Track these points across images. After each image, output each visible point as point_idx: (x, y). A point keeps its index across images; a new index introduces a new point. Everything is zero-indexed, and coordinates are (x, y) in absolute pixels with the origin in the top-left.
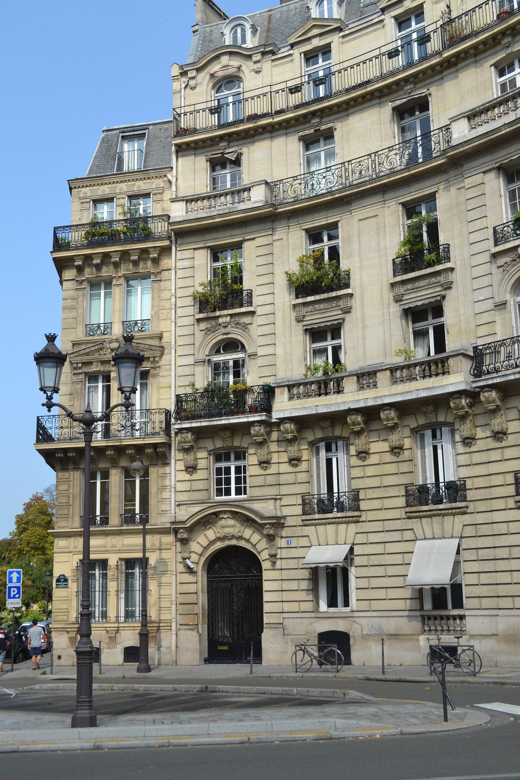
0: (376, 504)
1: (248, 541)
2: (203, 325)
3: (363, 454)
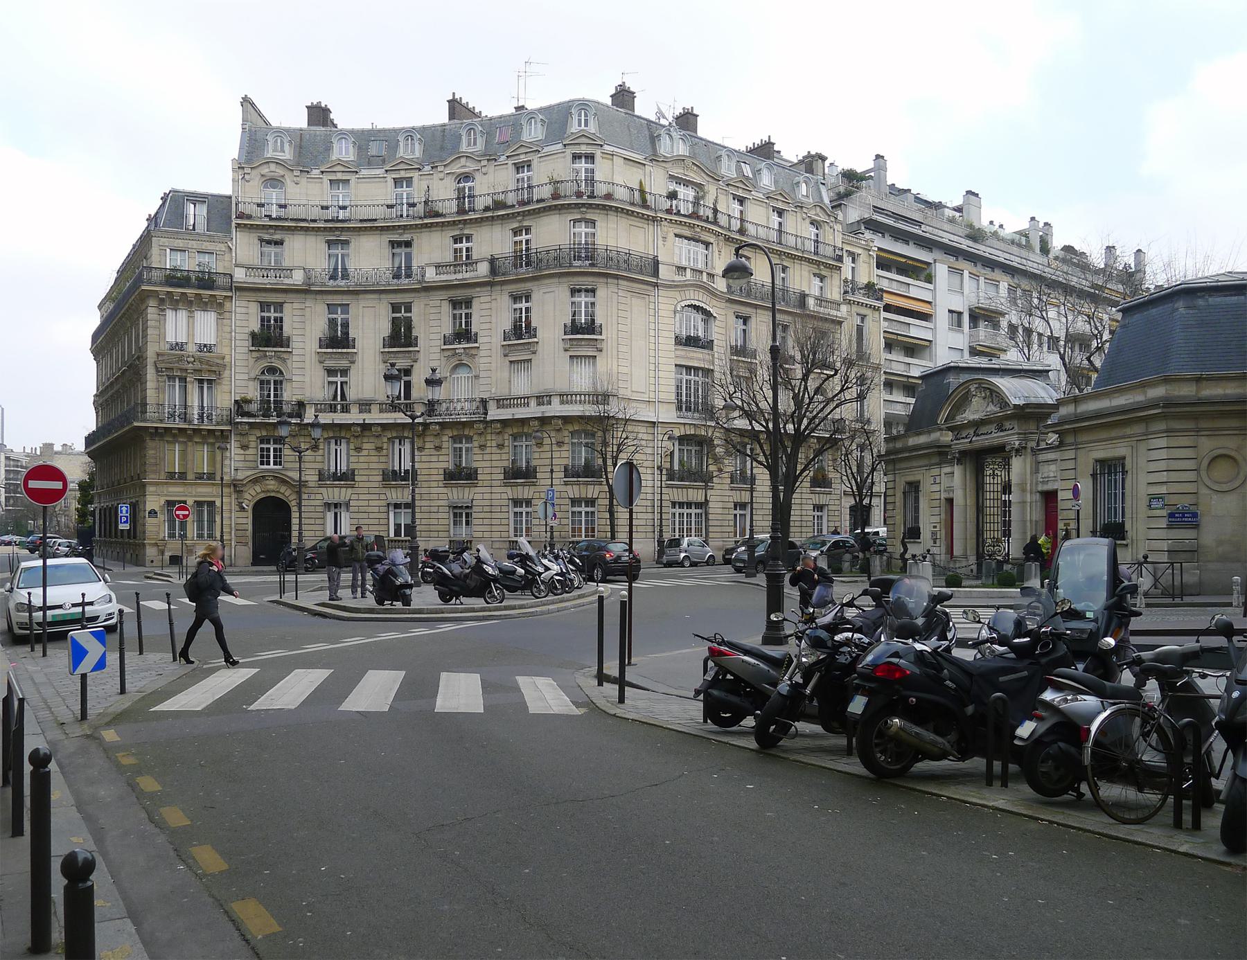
0: (365, 478)
2: (255, 355)
3: (358, 449)
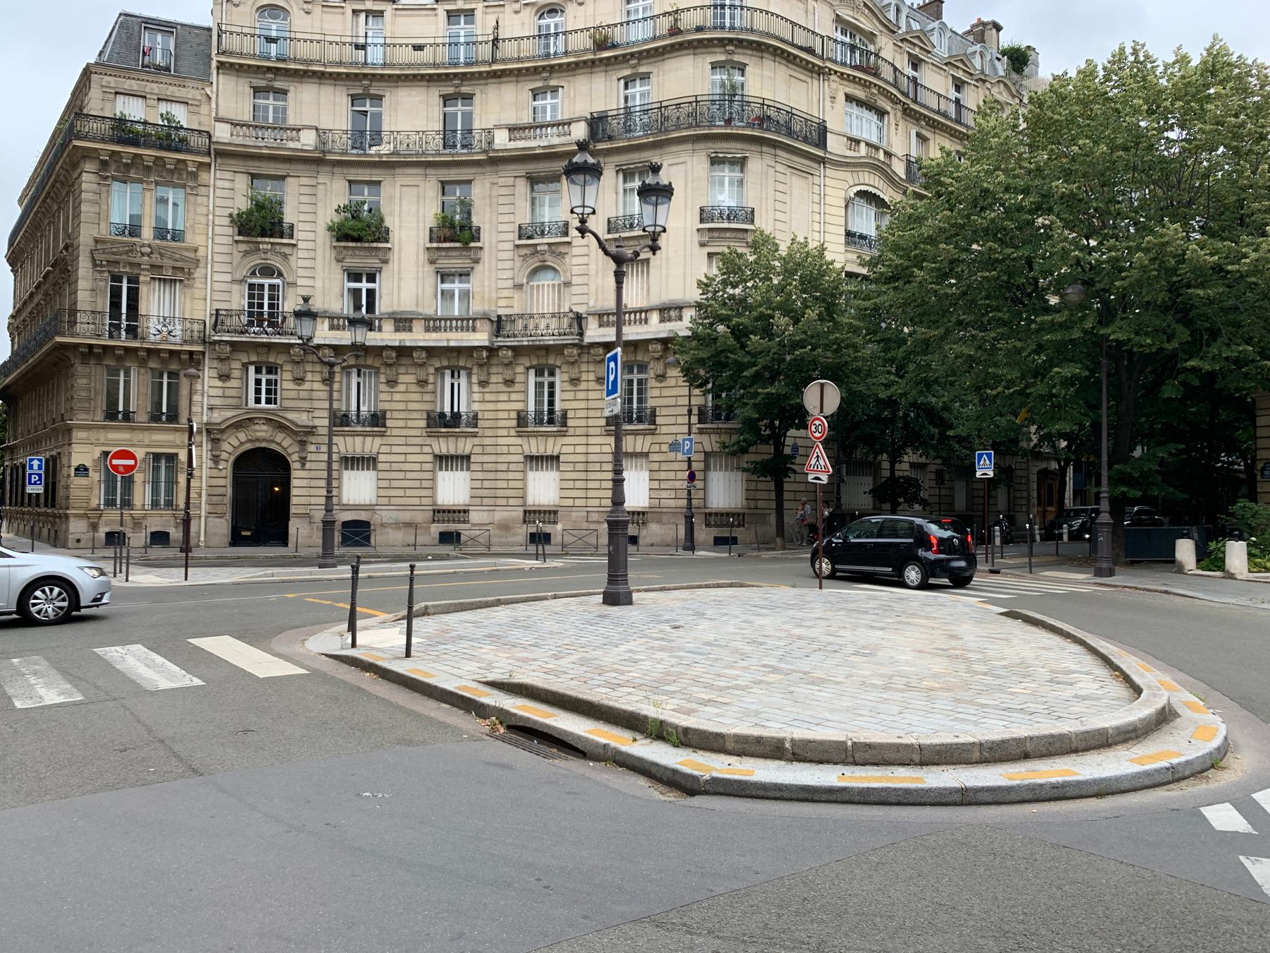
1: (279, 444)
2: (242, 247)
